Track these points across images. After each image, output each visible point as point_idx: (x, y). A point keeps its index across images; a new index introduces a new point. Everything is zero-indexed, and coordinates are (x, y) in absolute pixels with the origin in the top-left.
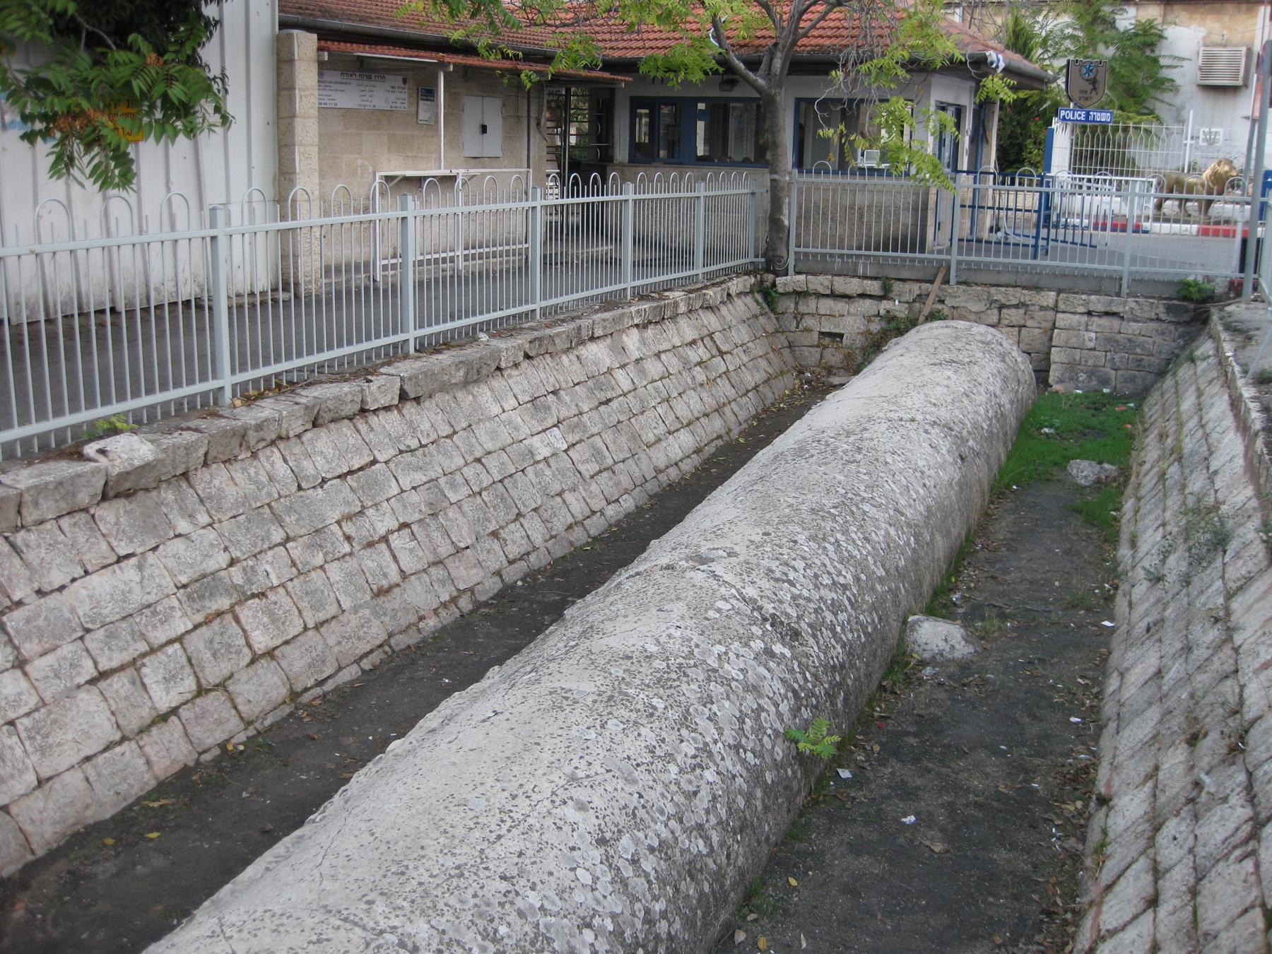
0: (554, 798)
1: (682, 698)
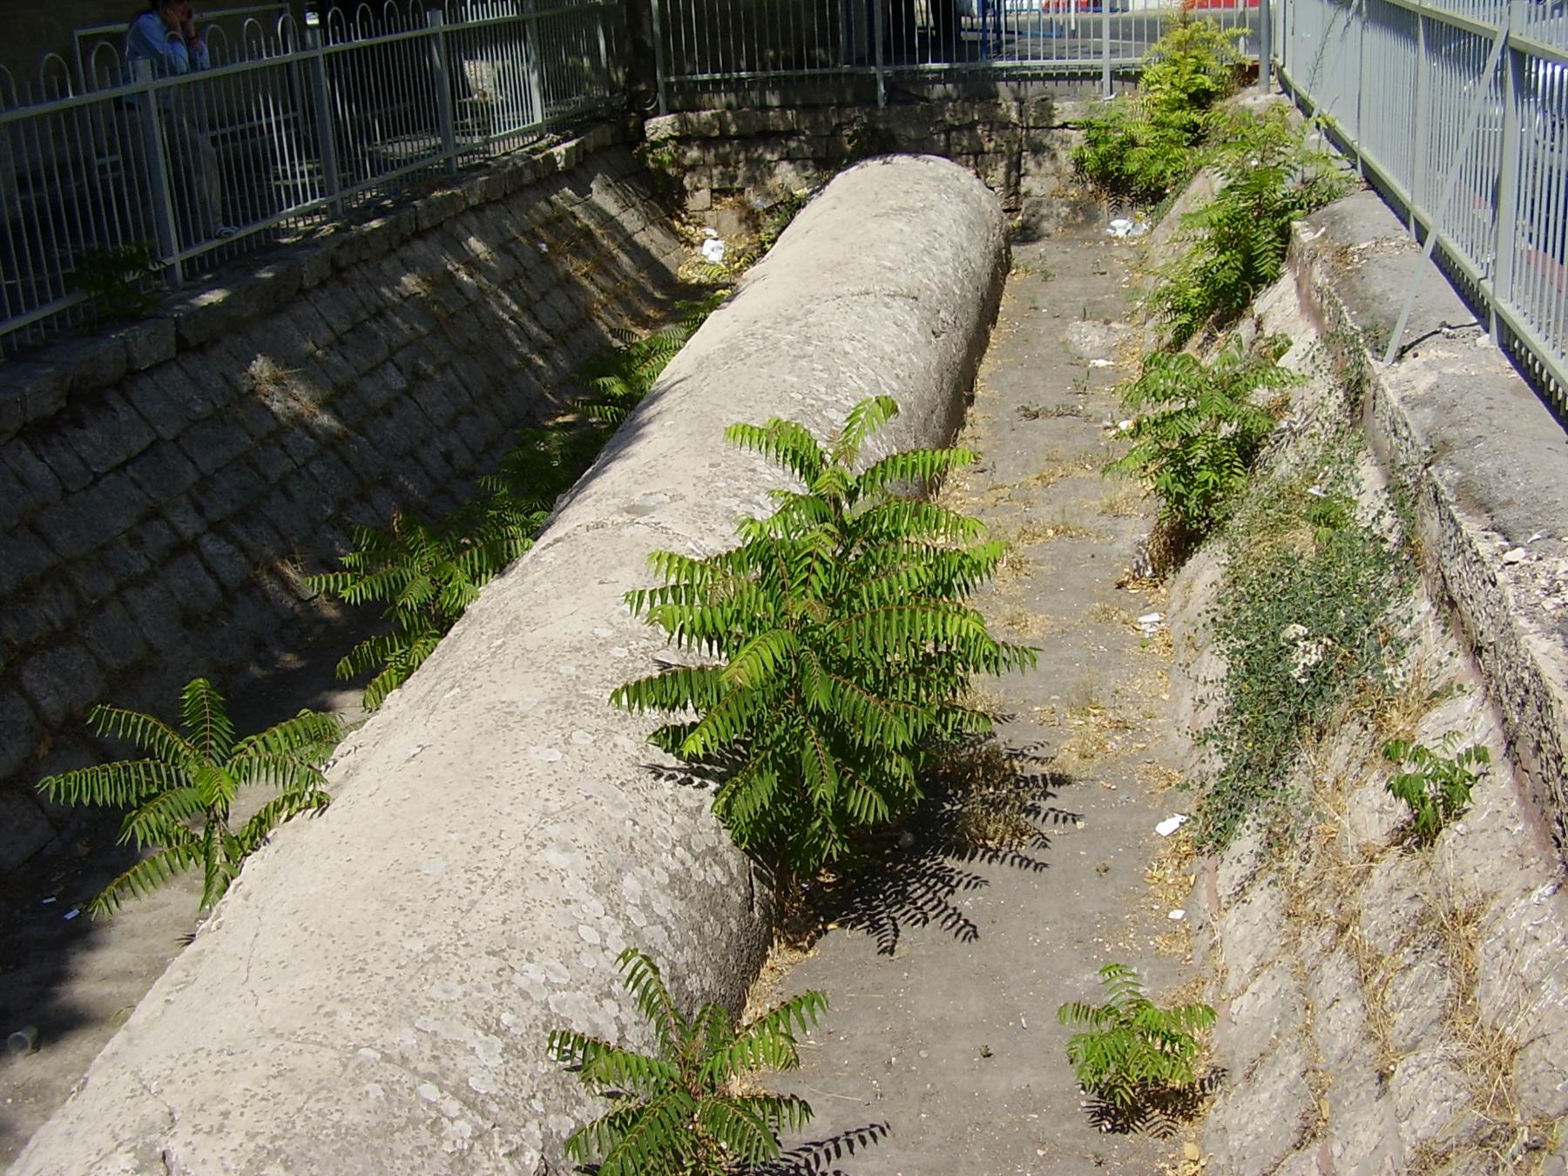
0: (529, 842)
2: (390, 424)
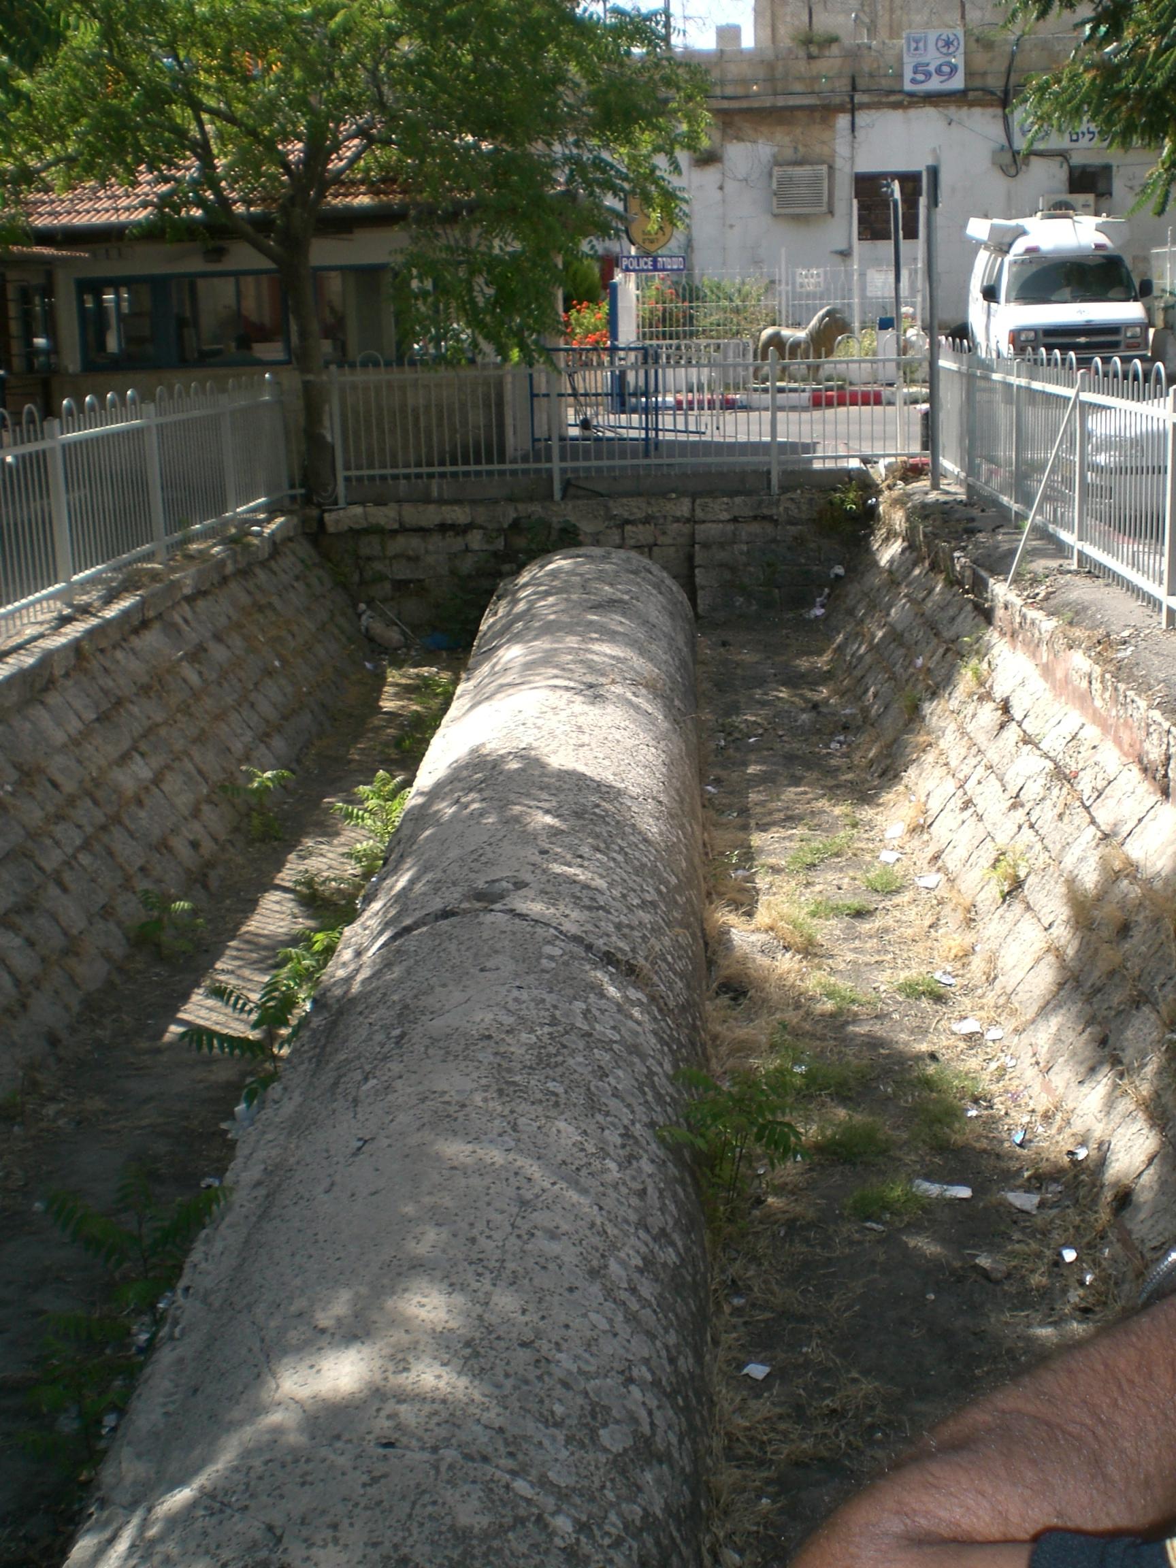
0: (517, 1232)
1: (576, 1076)
2: (142, 814)
